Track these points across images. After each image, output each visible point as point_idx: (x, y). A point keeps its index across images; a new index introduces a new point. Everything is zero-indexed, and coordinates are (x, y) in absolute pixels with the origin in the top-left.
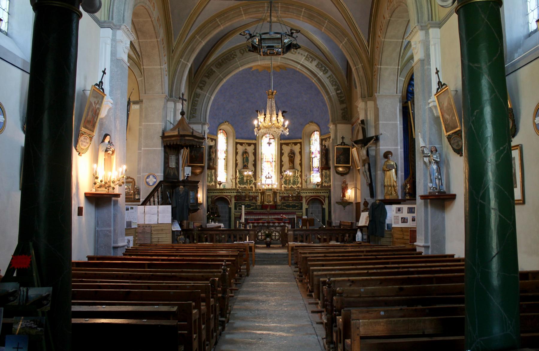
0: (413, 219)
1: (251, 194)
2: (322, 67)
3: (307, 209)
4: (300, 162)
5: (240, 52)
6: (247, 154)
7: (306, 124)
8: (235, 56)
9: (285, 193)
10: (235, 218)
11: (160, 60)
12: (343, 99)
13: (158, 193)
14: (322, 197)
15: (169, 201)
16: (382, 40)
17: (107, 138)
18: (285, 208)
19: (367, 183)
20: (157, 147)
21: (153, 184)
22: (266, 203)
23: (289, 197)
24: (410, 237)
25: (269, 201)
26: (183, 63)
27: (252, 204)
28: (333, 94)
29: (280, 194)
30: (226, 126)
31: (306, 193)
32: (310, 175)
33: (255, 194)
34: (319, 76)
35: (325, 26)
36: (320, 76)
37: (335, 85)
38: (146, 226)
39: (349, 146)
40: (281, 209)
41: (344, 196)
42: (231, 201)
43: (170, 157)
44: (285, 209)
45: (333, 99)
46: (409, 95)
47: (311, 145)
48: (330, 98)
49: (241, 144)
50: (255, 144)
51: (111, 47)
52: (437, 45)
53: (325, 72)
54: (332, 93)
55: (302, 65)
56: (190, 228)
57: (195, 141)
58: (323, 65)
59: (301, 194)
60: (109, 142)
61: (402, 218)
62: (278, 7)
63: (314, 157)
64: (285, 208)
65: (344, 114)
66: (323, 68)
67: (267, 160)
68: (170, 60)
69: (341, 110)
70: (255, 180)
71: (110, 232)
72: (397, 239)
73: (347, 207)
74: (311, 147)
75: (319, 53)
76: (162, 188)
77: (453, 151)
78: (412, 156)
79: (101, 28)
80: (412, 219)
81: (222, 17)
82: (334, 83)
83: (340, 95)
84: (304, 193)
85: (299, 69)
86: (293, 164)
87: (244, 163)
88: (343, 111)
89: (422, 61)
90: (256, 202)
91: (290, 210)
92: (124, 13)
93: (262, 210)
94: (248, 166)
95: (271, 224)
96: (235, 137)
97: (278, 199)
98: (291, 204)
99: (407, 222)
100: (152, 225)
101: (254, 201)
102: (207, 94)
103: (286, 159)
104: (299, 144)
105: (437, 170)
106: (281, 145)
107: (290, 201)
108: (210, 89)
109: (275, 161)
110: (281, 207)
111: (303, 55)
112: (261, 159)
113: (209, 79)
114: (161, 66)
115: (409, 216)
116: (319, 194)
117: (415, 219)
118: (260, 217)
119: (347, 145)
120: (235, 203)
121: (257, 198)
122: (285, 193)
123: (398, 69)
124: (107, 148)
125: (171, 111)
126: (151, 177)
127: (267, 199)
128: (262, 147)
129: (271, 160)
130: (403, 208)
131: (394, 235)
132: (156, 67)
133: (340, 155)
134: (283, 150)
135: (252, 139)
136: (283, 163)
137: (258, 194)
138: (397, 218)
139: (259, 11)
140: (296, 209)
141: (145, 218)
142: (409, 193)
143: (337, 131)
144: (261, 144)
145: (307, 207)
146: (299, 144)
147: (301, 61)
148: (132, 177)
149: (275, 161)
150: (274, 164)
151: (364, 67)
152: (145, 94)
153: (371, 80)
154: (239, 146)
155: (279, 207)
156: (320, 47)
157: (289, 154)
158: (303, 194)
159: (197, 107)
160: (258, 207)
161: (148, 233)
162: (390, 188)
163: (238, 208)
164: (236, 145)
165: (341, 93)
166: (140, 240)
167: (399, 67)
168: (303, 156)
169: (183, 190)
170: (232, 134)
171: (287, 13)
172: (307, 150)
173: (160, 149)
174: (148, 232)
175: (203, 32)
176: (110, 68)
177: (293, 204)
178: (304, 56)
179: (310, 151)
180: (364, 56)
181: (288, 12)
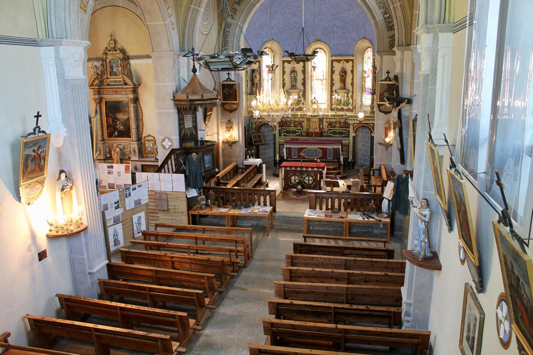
3: (354, 137)
6: (295, 73)
7: (359, 40)
9: (332, 119)
10: (280, 145)
11: (162, 15)
13: (171, 160)
14: (370, 124)
15: (183, 167)
18: (331, 134)
20: (169, 110)
21: (169, 148)
22: (311, 130)
23: (336, 123)
25: (314, 127)
26: (194, 9)
27: (297, 131)
28: (380, 18)
31: (354, 120)
33: (301, 119)
37: (383, 7)
38: (162, 193)
40: (327, 136)
43: (185, 118)
44: (331, 136)
45: (379, 25)
47: (364, 63)
48: (376, 23)
50: (352, 61)
51: (56, 68)
54: (378, 18)
56: (211, 186)
57: (207, 103)
59: (348, 121)
60: (66, 177)
64: (331, 134)
65: (392, 43)
67: (317, 78)
68: (178, 8)
70: (305, 99)
71: (84, 260)
74: (364, 66)
76: (174, 156)
82: (382, 5)
83: (388, 20)
84: (352, 120)
86: (345, 84)
87: (292, 83)
88: (391, 39)
89: (426, 76)
90: (301, 128)
91: (337, 138)
92: (65, 22)
93: (308, 137)
94: (296, 86)
96: (282, 55)
97: (325, 124)
98: (338, 131)
100: (168, 193)
103: (337, 77)
104: (351, 62)
106: (332, 61)
109: (326, 79)
110: (328, 134)
112: (312, 76)
113: (239, 6)
114: (164, 21)
116: (368, 121)
118: (303, 147)
120: (279, 129)
122: (332, 119)
124: (63, 186)
125: (184, 67)
126: (167, 140)
132: (159, 23)
133: (385, 92)
136: (334, 82)
137: (304, 120)
140: (343, 137)
141: (160, 186)
143: (382, 64)
145: (355, 135)
146: (351, 62)
148: (153, 135)
149: (326, 79)
150: (325, 81)
152: (153, 52)
153: (410, 23)
157: (340, 73)
158: (351, 121)
159: (228, 39)
160: (303, 134)
161: (165, 200)
166: (157, 206)
170: (278, 52)
173: (173, 112)
174: (164, 199)
177: (340, 131)
179: (363, 70)
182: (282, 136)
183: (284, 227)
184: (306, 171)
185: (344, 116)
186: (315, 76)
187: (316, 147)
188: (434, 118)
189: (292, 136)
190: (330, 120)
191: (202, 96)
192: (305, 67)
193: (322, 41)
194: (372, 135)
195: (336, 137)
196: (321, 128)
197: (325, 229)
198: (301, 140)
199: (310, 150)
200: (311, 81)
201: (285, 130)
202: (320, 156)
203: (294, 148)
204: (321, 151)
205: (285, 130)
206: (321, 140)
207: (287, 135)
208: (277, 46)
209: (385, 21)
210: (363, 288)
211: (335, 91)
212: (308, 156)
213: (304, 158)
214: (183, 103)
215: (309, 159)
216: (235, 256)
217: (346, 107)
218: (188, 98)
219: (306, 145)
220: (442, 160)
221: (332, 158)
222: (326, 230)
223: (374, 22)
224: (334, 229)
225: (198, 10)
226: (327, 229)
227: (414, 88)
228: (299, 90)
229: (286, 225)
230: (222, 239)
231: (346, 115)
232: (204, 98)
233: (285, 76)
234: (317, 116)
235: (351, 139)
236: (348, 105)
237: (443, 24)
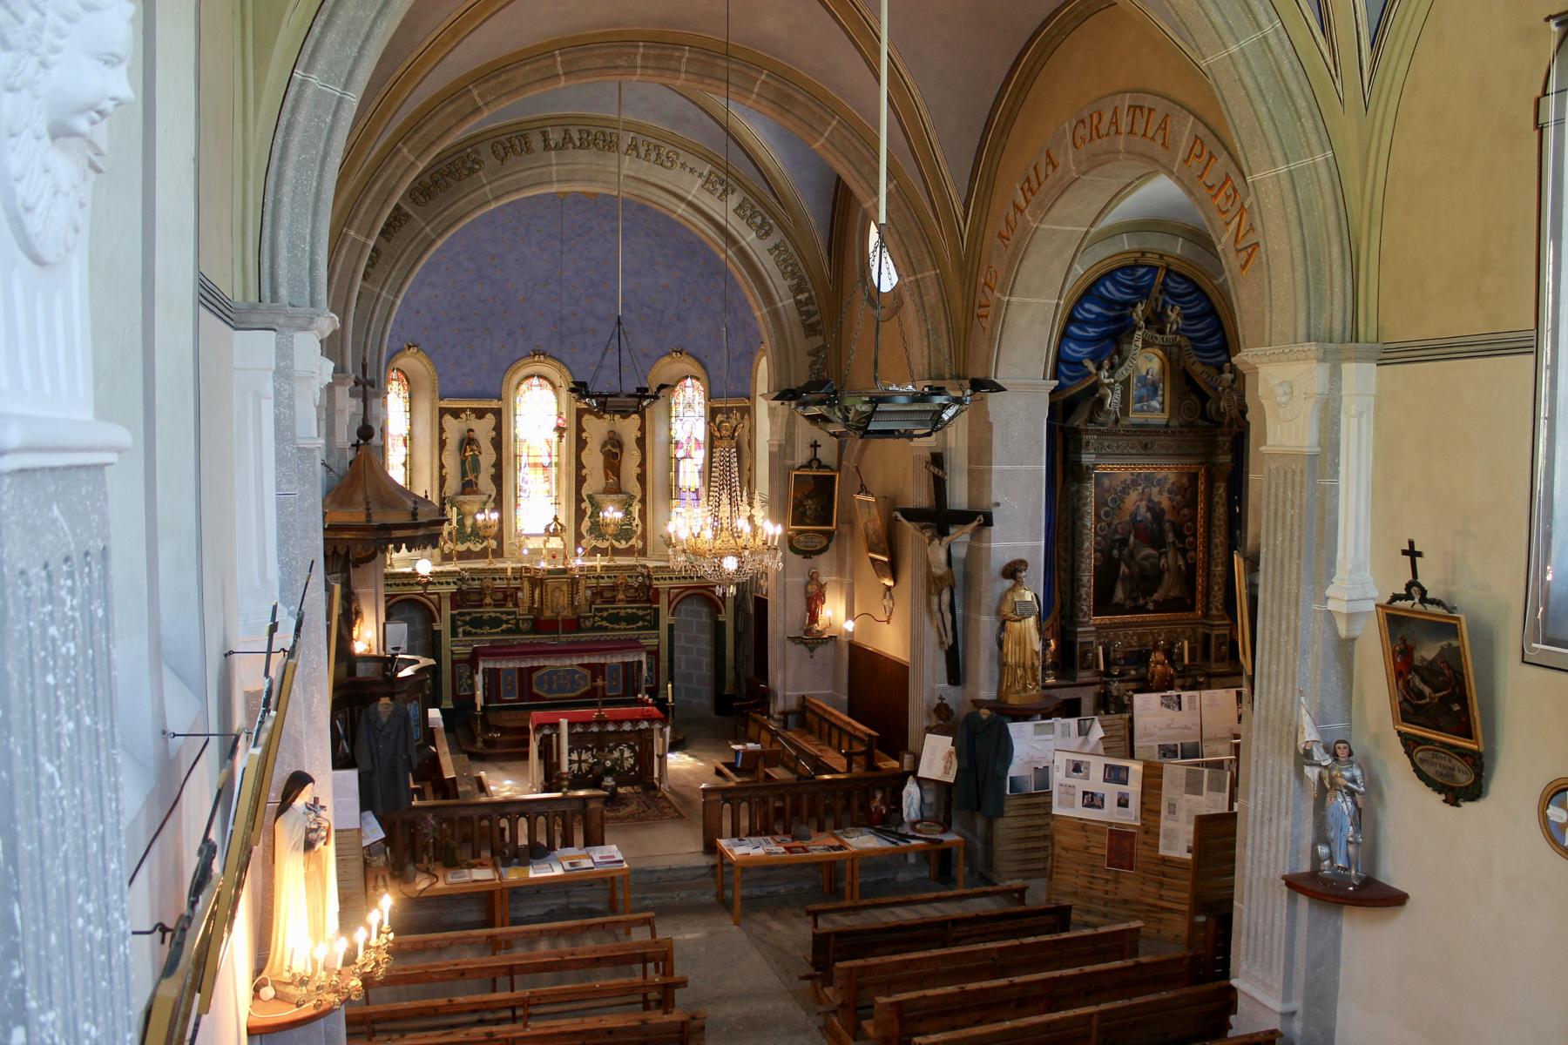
0: (1122, 801)
1: (498, 581)
2: (754, 214)
3: (671, 628)
4: (639, 471)
5: (494, 152)
6: (475, 448)
8: (477, 167)
10: (454, 663)
12: (813, 319)
16: (1032, 224)
17: (303, 792)
18: (605, 623)
19: (942, 643)
23: (614, 588)
24: (1109, 851)
25: (559, 603)
27: (505, 617)
28: (785, 303)
29: (589, 581)
30: (412, 361)
31: (671, 578)
32: (670, 511)
34: (743, 243)
35: (826, 134)
36: (747, 243)
37: (793, 274)
39: (832, 470)
40: (594, 629)
41: (814, 618)
42: (439, 611)
44: (606, 629)
45: (784, 319)
46: (1063, 368)
47: (673, 420)
48: (775, 314)
49: (456, 413)
50: (498, 413)
52: (1365, 416)
53: (763, 232)
55: (691, 204)
58: (758, 208)
59: (655, 582)
61: (1085, 793)
62: (680, 58)
63: (683, 458)
64: (605, 623)
66: (758, 220)
67: (532, 460)
69: (809, 354)
72: (1066, 849)
73: (819, 650)
75: (745, 170)
77: (1414, 775)
78: (1064, 554)
79: (236, 329)
80: (1119, 800)
81: (492, 83)
82: (789, 269)
83: (805, 308)
84: (665, 579)
85: (680, 216)
87: (464, 474)
91: (624, 632)
94: (476, 484)
95: (611, 728)
98: (623, 613)
99: (1101, 807)
101: (510, 607)
102: (384, 293)
103: (594, 459)
104: (490, 416)
105: (1354, 819)
107: (619, 601)
108: (393, 275)
109: (557, 465)
110: (594, 622)
111: (696, 174)
112: (516, 456)
115: (1111, 791)
117: (1127, 801)
118: (536, 664)
119: (826, 467)
120: (452, 615)
121: (520, 594)
122: (603, 578)
123: (1058, 305)
124: (309, 831)
127: (552, 601)
128: (518, 418)
129: (546, 461)
130: (1089, 763)
131: (1057, 837)
133: (807, 497)
134: (584, 431)
135: (490, 397)
136: (584, 472)
138: (1071, 790)
139: (616, 67)
140: (639, 628)
142: (1054, 666)
144: (515, 409)
146: (490, 416)
147: (689, 193)
149: (557, 465)
150: (554, 470)
151: (941, 281)
154: (448, 418)
155: (588, 624)
156: (757, 155)
157: (604, 445)
158: (662, 581)
162: (1020, 672)
163: (461, 630)
164: (441, 417)
165: (809, 300)
167: (1062, 302)
168: (648, 454)
169: (391, 709)
170: (427, 384)
171: (707, 81)
172: (661, 437)
175: (422, 133)
176: (278, 489)
177: (629, 611)
178: (700, 175)
180: (945, 246)
181: (709, 77)
182: (461, 635)
183: (647, 902)
184: (614, 732)
185: (639, 569)
186: (525, 454)
187: (576, 661)
188: (1336, 553)
189: (489, 634)
190: (508, 584)
191: (414, 514)
192: (501, 429)
193: (550, 356)
194: (436, 628)
195: (620, 630)
196: (577, 607)
197: (766, 890)
198: (520, 645)
199: (555, 672)
200: (516, 470)
201: (468, 618)
202: (586, 688)
203: (508, 670)
204: (588, 673)
205: (468, 618)
206: (579, 642)
207: (473, 631)
208: (425, 366)
209: (798, 309)
210: (1137, 1006)
211: (590, 497)
212: (550, 691)
213: (539, 698)
214: (345, 536)
215: (552, 699)
216: (641, 1006)
217: (623, 542)
218: (370, 521)
219: (545, 658)
220: (1353, 647)
221: (621, 693)
222: (770, 893)
223: (768, 312)
224: (793, 887)
225: (915, 274)
226: (772, 889)
227: (993, 486)
228: (484, 498)
229: (654, 895)
230: (598, 959)
231: (644, 566)
232: (421, 519)
233: (446, 454)
234: (564, 571)
235: (663, 630)
236: (630, 539)
237: (1353, 344)
